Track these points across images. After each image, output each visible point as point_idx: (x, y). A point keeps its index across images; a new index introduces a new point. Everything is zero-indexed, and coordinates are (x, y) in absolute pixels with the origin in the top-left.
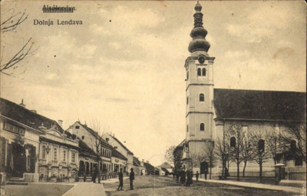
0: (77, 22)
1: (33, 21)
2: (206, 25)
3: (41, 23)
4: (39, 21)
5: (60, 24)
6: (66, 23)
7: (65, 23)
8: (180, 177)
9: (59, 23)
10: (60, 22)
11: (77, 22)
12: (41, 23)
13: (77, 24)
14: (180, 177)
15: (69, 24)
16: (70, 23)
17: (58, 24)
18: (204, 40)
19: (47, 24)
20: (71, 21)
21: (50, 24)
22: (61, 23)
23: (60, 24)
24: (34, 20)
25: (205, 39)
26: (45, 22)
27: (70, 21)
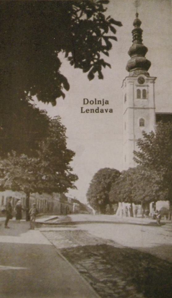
0: (105, 110)
1: (83, 100)
2: (146, 41)
3: (92, 102)
4: (89, 101)
5: (84, 112)
6: (92, 111)
7: (90, 111)
8: (91, 9)
9: (83, 111)
10: (84, 110)
11: (105, 110)
12: (92, 102)
13: (106, 111)
14: (91, 9)
15: (96, 112)
16: (97, 111)
17: (82, 112)
18: (144, 58)
19: (101, 103)
20: (98, 109)
21: (104, 104)
22: (85, 110)
23: (84, 112)
24: (84, 99)
25: (145, 58)
26: (98, 101)
27: (97, 108)
